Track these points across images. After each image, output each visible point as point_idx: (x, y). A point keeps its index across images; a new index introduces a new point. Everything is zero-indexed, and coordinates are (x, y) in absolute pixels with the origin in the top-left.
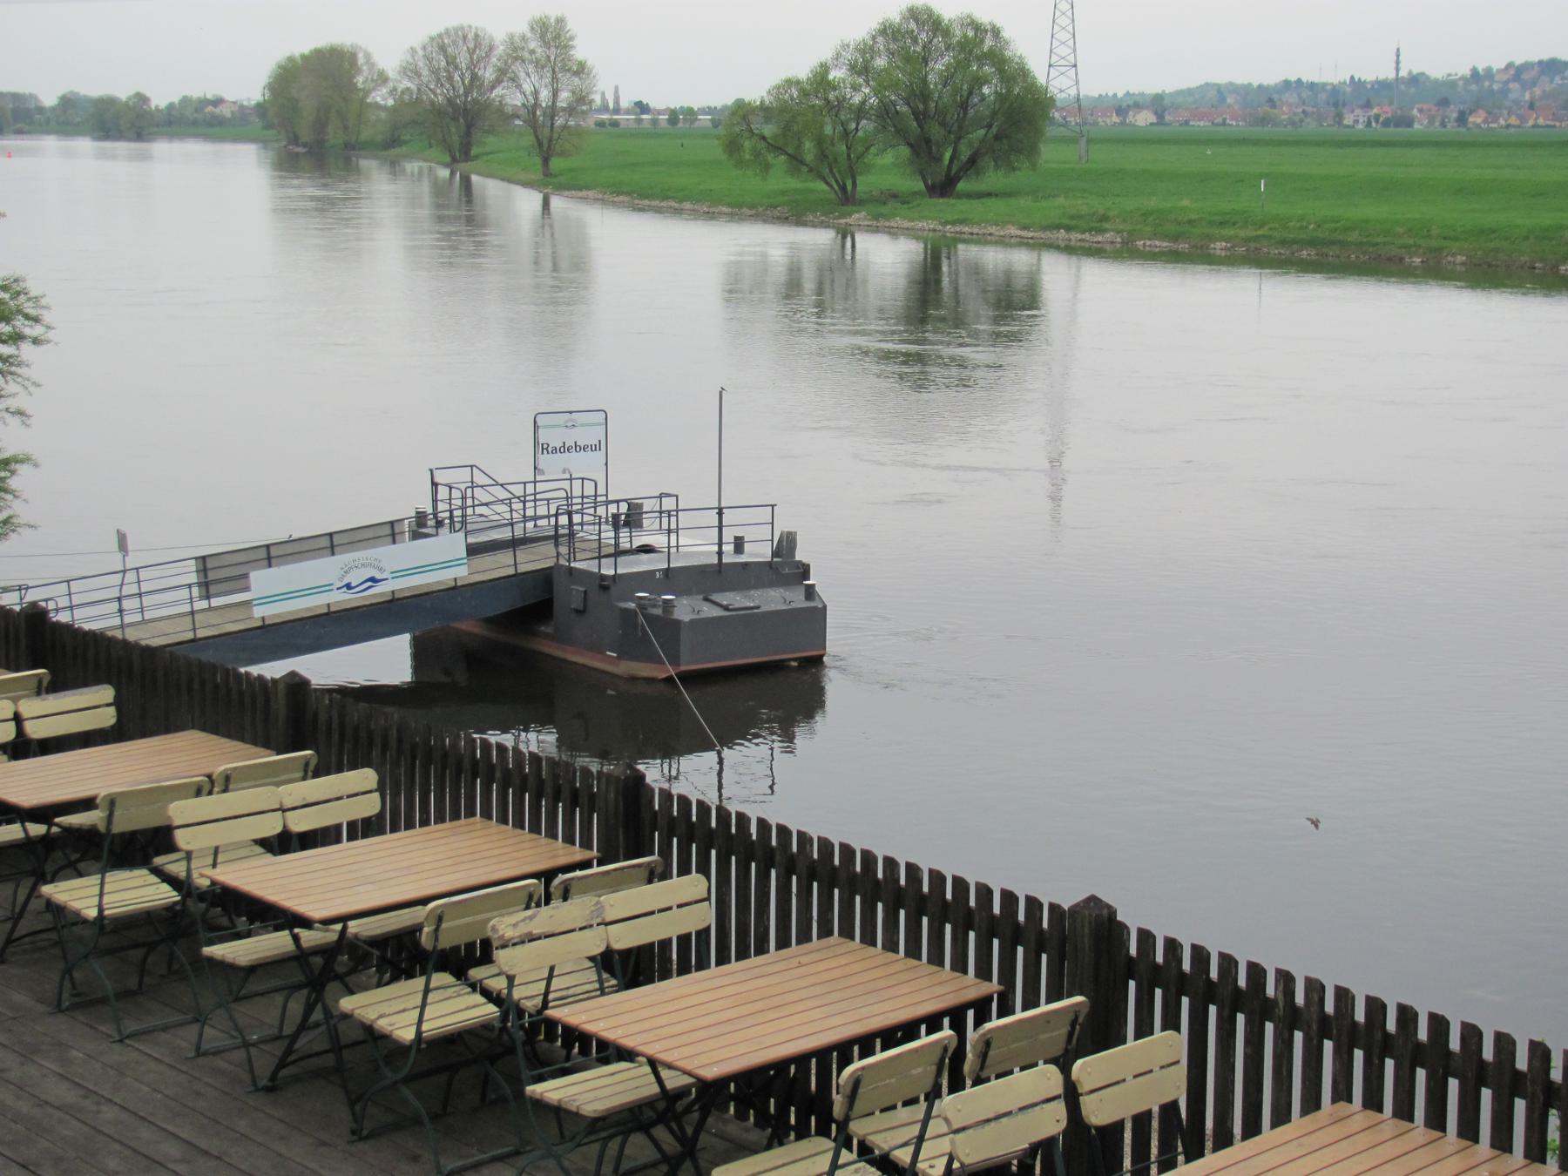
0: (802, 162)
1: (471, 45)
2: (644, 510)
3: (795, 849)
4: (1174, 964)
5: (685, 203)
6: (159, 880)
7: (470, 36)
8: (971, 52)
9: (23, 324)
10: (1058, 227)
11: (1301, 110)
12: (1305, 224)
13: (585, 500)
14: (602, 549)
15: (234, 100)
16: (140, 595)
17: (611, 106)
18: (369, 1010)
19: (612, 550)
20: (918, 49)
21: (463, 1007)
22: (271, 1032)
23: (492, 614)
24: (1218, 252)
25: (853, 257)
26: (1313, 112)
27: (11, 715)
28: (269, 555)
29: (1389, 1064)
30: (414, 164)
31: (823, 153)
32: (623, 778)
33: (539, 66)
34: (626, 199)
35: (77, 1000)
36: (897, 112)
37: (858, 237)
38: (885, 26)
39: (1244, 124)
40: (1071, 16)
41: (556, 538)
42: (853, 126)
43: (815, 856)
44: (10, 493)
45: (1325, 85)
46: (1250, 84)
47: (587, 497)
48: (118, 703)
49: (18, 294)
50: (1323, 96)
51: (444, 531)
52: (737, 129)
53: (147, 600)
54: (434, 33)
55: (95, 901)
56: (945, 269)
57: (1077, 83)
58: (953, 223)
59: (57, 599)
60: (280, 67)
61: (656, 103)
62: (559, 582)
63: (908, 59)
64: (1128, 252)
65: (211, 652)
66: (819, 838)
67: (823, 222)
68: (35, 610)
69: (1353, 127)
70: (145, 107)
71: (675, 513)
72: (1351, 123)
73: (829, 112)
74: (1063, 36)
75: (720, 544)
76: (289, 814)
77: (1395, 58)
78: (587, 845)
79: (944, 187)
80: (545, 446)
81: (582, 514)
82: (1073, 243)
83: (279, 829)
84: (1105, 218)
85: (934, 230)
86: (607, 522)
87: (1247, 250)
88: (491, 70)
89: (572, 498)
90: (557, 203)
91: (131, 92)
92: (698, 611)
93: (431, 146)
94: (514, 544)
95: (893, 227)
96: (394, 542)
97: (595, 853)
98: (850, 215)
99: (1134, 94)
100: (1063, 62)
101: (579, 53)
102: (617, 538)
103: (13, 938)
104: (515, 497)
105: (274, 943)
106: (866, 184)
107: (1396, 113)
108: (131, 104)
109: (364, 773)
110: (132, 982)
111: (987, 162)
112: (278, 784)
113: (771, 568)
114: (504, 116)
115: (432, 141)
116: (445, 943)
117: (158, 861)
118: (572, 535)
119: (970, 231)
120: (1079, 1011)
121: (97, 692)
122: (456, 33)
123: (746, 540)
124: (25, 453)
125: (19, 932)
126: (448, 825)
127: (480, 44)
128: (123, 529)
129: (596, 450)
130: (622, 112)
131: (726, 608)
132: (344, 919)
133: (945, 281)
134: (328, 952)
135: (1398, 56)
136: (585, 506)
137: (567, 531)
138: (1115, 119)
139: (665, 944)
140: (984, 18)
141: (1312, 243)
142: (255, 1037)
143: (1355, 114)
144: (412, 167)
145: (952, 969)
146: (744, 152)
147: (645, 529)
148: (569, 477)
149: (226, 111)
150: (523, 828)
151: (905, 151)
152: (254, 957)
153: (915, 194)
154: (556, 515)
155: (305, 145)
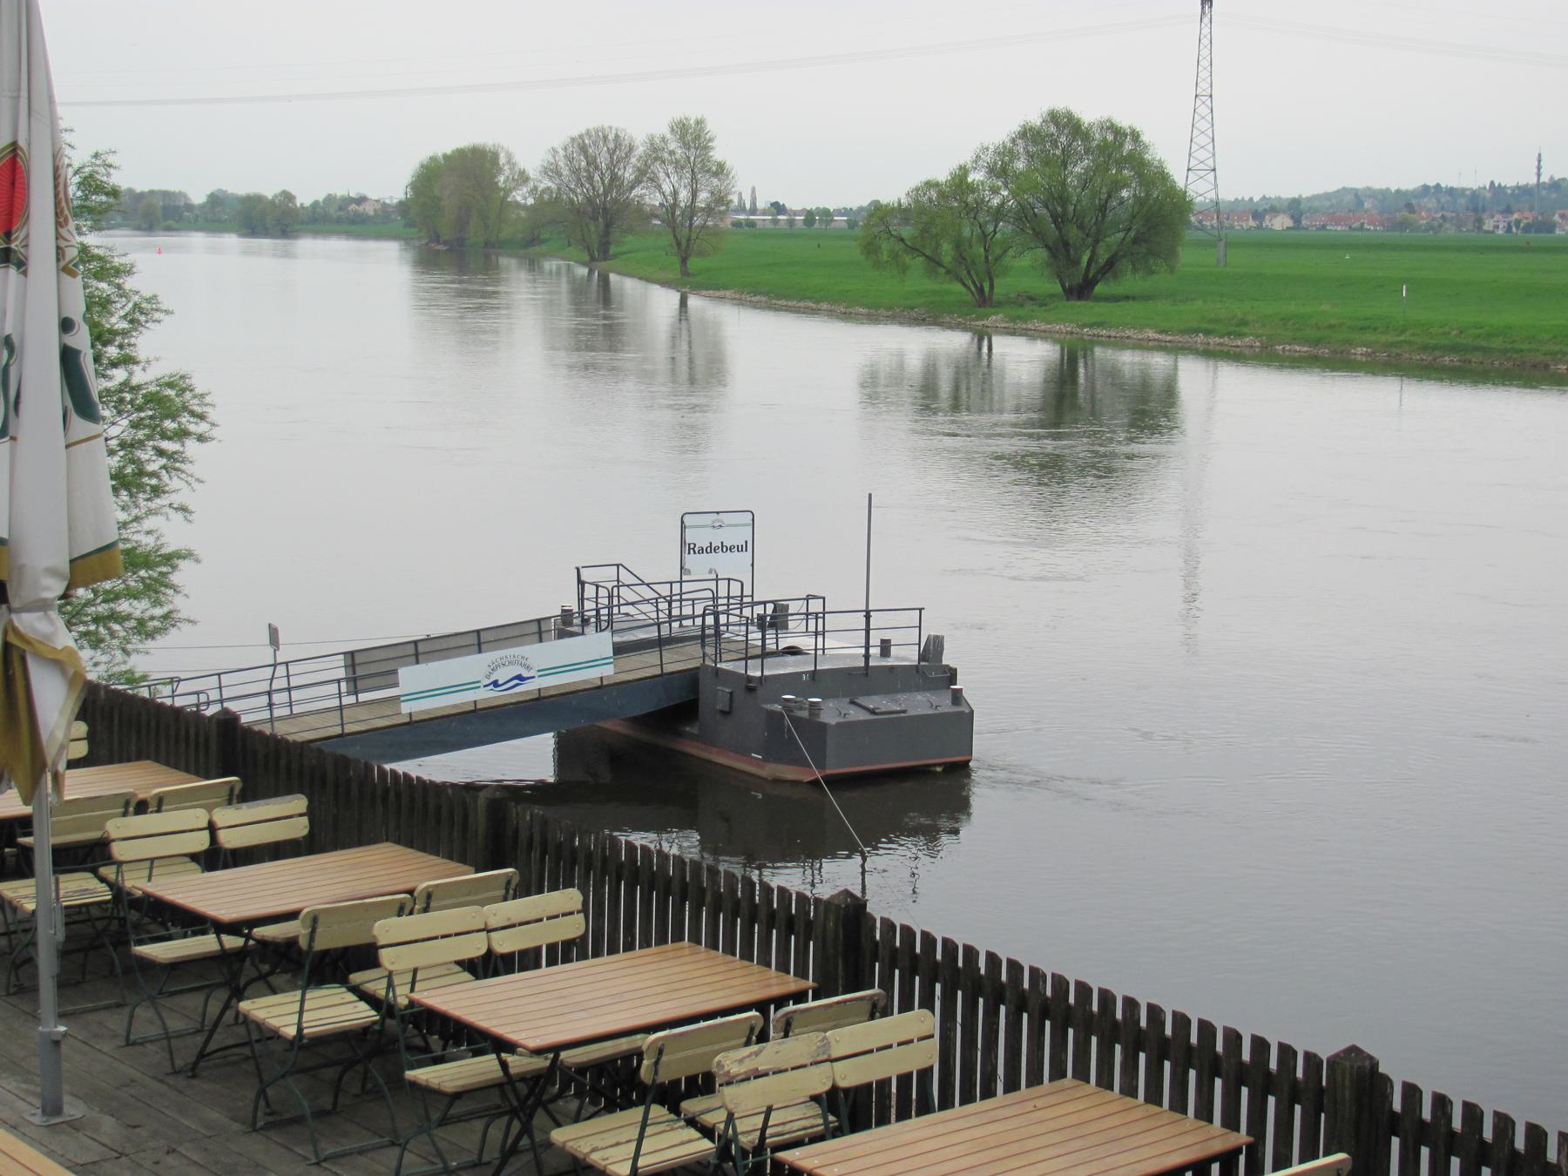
0: (940, 264)
1: (611, 145)
2: (790, 612)
3: (1026, 985)
4: (1442, 1122)
5: (822, 304)
6: (355, 998)
7: (611, 137)
8: (1110, 156)
9: (188, 421)
10: (1196, 331)
11: (1440, 215)
12: (1447, 330)
13: (731, 601)
14: (749, 650)
15: (376, 199)
16: (289, 689)
17: (748, 206)
18: (582, 1142)
19: (759, 651)
20: (1058, 152)
21: (678, 1141)
22: (470, 1159)
23: (638, 712)
24: (1359, 358)
25: (989, 365)
26: (1452, 218)
27: (205, 824)
28: (418, 651)
29: (1425, 1152)
30: (555, 262)
31: (961, 255)
32: (843, 906)
33: (679, 166)
34: (764, 299)
35: (270, 1119)
36: (1035, 214)
37: (994, 339)
38: (1025, 129)
39: (1382, 228)
40: (1210, 120)
41: (703, 638)
42: (990, 228)
43: (1049, 993)
44: (171, 588)
45: (1463, 190)
46: (1388, 189)
47: (733, 598)
48: (310, 813)
49: (183, 390)
50: (1462, 201)
51: (590, 629)
52: (875, 230)
53: (296, 695)
54: (575, 134)
55: (295, 1018)
56: (1081, 370)
57: (1216, 186)
58: (1091, 326)
59: (209, 692)
60: (422, 166)
61: (793, 204)
62: (705, 684)
63: (1046, 163)
64: (1268, 356)
65: (358, 748)
66: (1053, 975)
67: (960, 324)
68: (227, 717)
69: (1493, 232)
70: (290, 205)
71: (822, 615)
72: (1491, 229)
73: (967, 214)
74: (1202, 140)
75: (867, 647)
76: (493, 934)
77: (1537, 163)
78: (801, 973)
79: (1081, 290)
80: (692, 546)
81: (728, 615)
82: (1211, 347)
83: (483, 951)
84: (1243, 323)
85: (1072, 333)
86: (752, 624)
87: (1389, 356)
88: (631, 170)
89: (718, 598)
90: (694, 302)
91: (278, 190)
92: (845, 715)
93: (570, 245)
94: (660, 643)
95: (1031, 330)
96: (541, 641)
97: (810, 982)
98: (987, 317)
99: (1270, 198)
100: (1202, 166)
101: (717, 155)
102: (763, 639)
103: (206, 1052)
104: (661, 597)
105: (483, 1067)
106: (1003, 286)
107: (1537, 218)
108: (277, 201)
109: (569, 893)
110: (326, 1102)
111: (1124, 265)
112: (483, 903)
113: (918, 671)
114: (642, 215)
115: (571, 240)
116: (665, 1077)
117: (356, 978)
118: (718, 634)
119: (1108, 334)
120: (1341, 1169)
121: (290, 802)
122: (597, 133)
123: (892, 643)
124: (187, 548)
125: (212, 1047)
126: (654, 949)
127: (620, 145)
128: (276, 624)
129: (742, 550)
130: (758, 213)
131: (873, 712)
132: (557, 1049)
133: (1081, 380)
134: (537, 1080)
135: (1539, 161)
136: (731, 607)
137: (712, 632)
138: (1252, 223)
139: (884, 1084)
140: (1124, 122)
141: (1454, 349)
142: (454, 1164)
143: (1495, 219)
144: (550, 265)
145: (1197, 1116)
146: (882, 253)
147: (791, 631)
148: (714, 577)
149: (369, 209)
150: (734, 954)
151: (1042, 254)
152: (461, 1083)
153: (1052, 296)
154: (703, 616)
155: (445, 243)
